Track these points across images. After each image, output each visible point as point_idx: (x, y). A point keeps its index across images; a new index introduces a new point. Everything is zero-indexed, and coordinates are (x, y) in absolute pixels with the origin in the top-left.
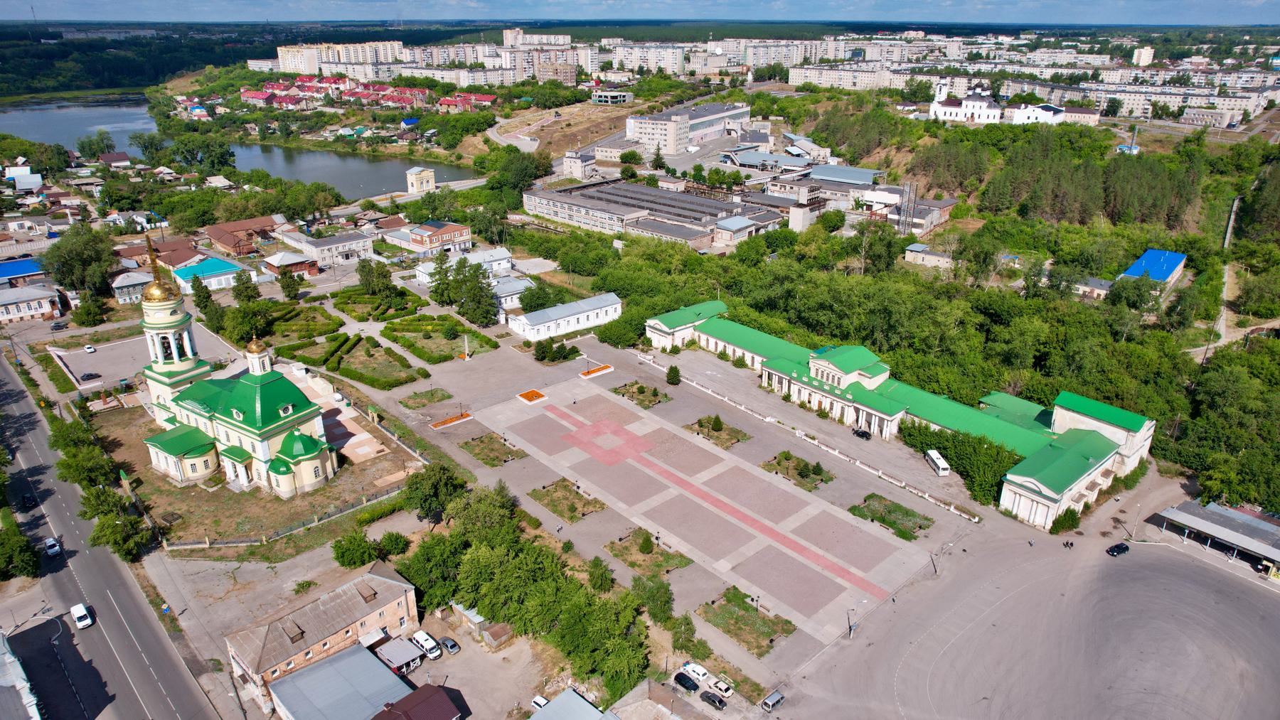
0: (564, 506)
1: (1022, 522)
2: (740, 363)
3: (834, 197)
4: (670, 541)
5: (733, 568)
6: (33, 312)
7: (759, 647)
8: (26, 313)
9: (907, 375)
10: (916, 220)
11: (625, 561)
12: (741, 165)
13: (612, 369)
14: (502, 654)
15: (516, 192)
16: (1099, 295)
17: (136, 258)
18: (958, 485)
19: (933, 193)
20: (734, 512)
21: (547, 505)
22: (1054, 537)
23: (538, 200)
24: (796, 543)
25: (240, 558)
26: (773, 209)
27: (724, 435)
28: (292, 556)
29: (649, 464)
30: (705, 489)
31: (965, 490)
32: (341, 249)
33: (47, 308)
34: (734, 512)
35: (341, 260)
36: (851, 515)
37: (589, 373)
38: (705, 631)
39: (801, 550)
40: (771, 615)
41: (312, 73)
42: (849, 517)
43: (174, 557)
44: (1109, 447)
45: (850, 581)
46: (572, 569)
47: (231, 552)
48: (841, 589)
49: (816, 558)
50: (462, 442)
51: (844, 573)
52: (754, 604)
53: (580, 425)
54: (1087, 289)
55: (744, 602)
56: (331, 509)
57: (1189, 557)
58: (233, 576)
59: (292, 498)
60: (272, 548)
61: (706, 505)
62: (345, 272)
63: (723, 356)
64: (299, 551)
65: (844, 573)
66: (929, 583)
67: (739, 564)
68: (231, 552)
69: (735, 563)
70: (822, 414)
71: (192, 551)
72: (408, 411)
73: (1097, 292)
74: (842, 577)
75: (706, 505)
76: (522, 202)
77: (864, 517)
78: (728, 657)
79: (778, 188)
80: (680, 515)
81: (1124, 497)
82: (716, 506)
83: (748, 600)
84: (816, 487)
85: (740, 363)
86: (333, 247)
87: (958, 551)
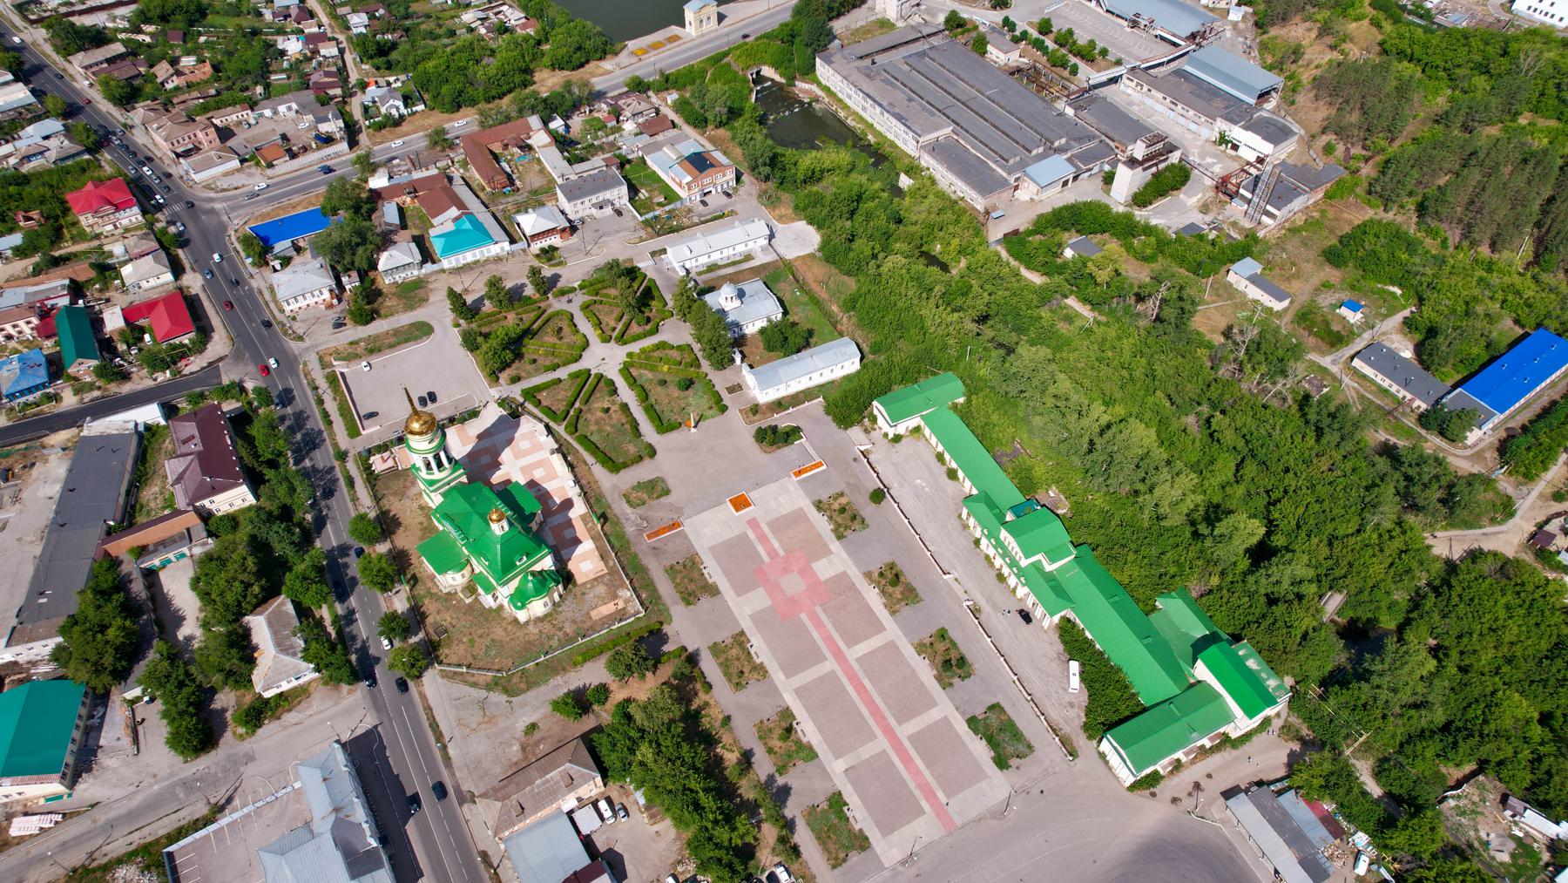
0: (734, 670)
1: (1110, 769)
2: (952, 474)
3: (1197, 120)
4: (808, 730)
5: (847, 770)
6: (316, 299)
7: (836, 858)
8: (311, 301)
9: (1459, 36)
10: (1269, 208)
11: (766, 744)
12: (1108, 11)
13: (824, 467)
14: (656, 827)
15: (810, 50)
16: (1419, 407)
17: (397, 200)
18: (1079, 707)
19: (1325, 139)
20: (870, 703)
21: (721, 665)
22: (1128, 794)
23: (831, 71)
24: (907, 752)
25: (489, 687)
26: (1108, 141)
27: (897, 591)
28: (523, 691)
29: (818, 624)
30: (856, 667)
31: (1083, 715)
32: (594, 201)
33: (327, 295)
34: (870, 703)
35: (594, 211)
36: (965, 726)
37: (800, 472)
38: (803, 836)
39: (907, 760)
40: (857, 827)
41: (165, 570)
42: (962, 727)
43: (443, 677)
44: (1229, 718)
45: (932, 805)
46: (723, 747)
47: (481, 680)
48: (921, 812)
49: (916, 773)
50: (669, 564)
51: (930, 795)
52: (848, 813)
53: (773, 554)
54: (1409, 396)
55: (842, 811)
56: (555, 643)
57: (1230, 843)
58: (482, 705)
59: (527, 623)
60: (510, 681)
61: (850, 688)
62: (536, 351)
63: (940, 457)
64: (530, 686)
65: (930, 795)
66: (994, 823)
67: (852, 767)
68: (481, 680)
69: (850, 765)
70: (1001, 577)
71: (455, 673)
72: (629, 510)
73: (1417, 403)
74: (927, 800)
75: (850, 688)
76: (814, 65)
77: (976, 732)
78: (811, 864)
79: (1133, 84)
80: (824, 697)
81: (1227, 754)
82: (857, 691)
83: (845, 808)
84: (951, 685)
85: (952, 474)
86: (586, 200)
87: (1036, 792)
